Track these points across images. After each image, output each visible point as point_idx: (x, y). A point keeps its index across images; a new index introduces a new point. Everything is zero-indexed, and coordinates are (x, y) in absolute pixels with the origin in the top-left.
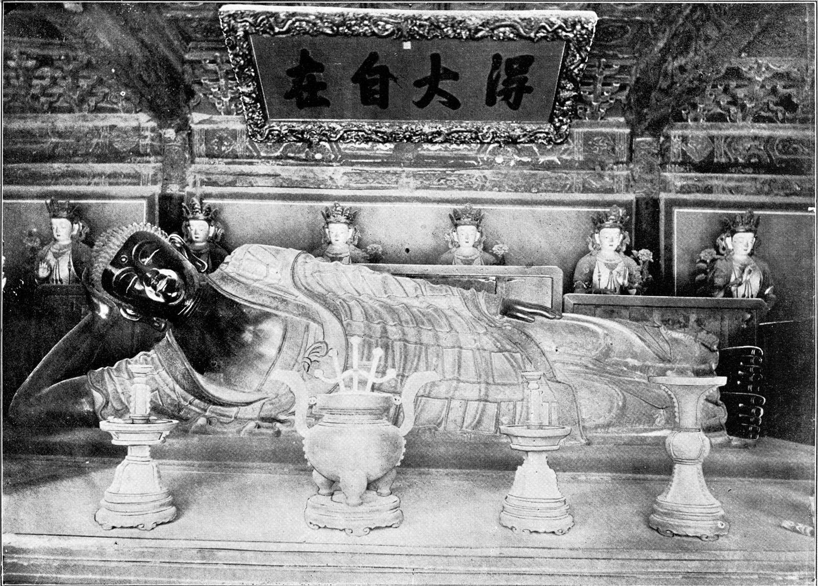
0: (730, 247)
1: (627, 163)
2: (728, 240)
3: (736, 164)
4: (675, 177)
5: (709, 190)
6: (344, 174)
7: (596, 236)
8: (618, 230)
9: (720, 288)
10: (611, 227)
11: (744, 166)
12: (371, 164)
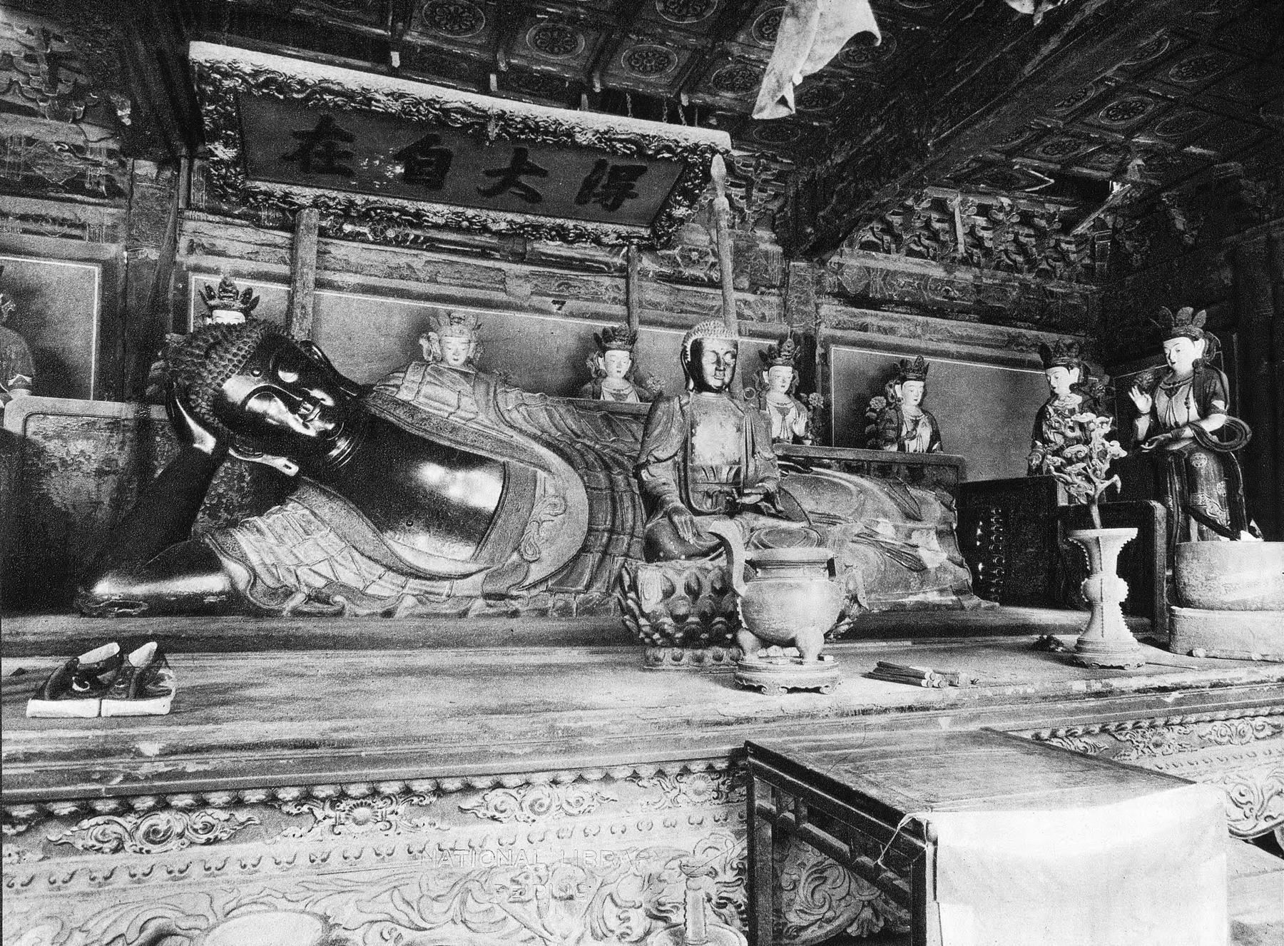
0: (899, 395)
1: (779, 288)
2: (897, 387)
3: (891, 301)
4: (830, 309)
5: (864, 328)
6: (428, 262)
7: (765, 374)
8: (790, 369)
9: (892, 442)
10: (783, 364)
11: (898, 304)
12: (465, 254)
